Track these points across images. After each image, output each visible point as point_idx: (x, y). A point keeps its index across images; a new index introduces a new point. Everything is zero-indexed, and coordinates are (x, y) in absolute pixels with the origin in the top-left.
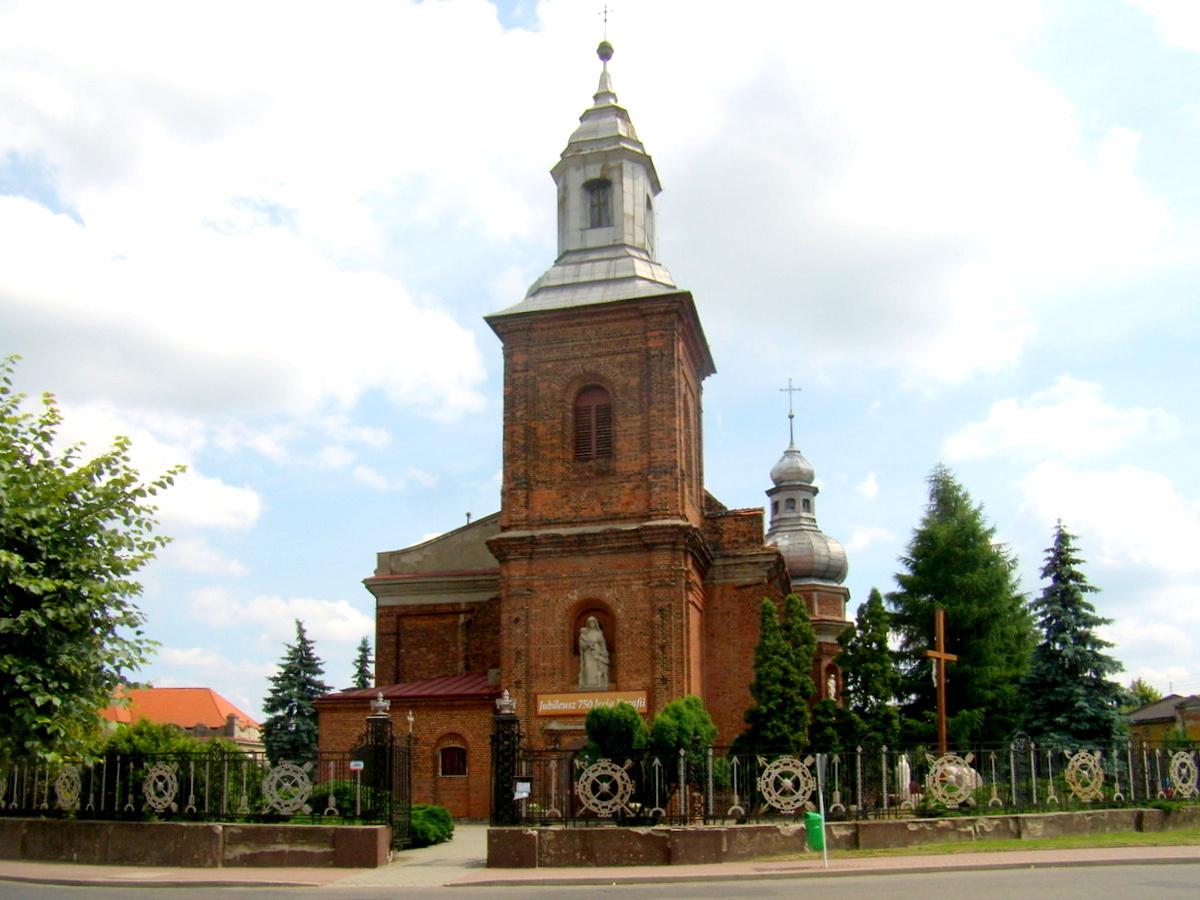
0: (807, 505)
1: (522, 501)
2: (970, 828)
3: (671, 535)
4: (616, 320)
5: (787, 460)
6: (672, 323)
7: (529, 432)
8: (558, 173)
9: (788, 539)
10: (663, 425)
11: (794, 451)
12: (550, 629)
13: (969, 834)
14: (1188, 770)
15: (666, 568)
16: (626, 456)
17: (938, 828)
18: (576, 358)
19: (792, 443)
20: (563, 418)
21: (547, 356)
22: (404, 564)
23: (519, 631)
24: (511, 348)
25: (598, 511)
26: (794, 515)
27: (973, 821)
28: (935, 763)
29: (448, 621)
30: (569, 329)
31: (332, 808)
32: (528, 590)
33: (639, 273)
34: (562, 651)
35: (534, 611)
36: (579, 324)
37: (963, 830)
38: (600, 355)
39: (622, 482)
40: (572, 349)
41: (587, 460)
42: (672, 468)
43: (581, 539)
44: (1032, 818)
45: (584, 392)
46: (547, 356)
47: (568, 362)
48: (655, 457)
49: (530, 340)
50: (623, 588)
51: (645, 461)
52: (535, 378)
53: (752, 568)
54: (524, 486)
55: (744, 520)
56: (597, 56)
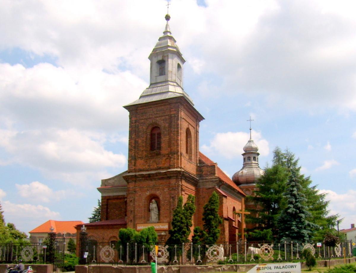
0: (254, 159)
1: (133, 164)
2: (220, 268)
3: (175, 174)
4: (162, 106)
5: (248, 144)
6: (179, 106)
7: (136, 142)
8: (150, 58)
9: (247, 170)
10: (175, 139)
11: (251, 141)
12: (141, 204)
13: (219, 270)
14: (339, 248)
15: (174, 184)
16: (164, 149)
17: (208, 268)
18: (150, 118)
19: (251, 138)
20: (146, 137)
21: (142, 118)
22: (109, 183)
23: (132, 204)
24: (132, 116)
25: (155, 166)
26: (250, 162)
27: (221, 266)
28: (209, 248)
29: (122, 201)
30: (148, 109)
31: (199, 260)
32: (134, 191)
33: (170, 90)
34: (144, 210)
35: (136, 198)
36: (151, 107)
37: (217, 269)
38: (157, 117)
39: (162, 157)
40: (149, 115)
41: (154, 150)
42: (177, 152)
43: (149, 176)
44: (241, 265)
45: (153, 129)
46: (142, 118)
47: (148, 120)
48: (172, 149)
49: (137, 113)
50: (162, 190)
51: (169, 150)
52: (138, 125)
53: (211, 183)
54: (134, 159)
55: (209, 167)
56: (165, 19)
